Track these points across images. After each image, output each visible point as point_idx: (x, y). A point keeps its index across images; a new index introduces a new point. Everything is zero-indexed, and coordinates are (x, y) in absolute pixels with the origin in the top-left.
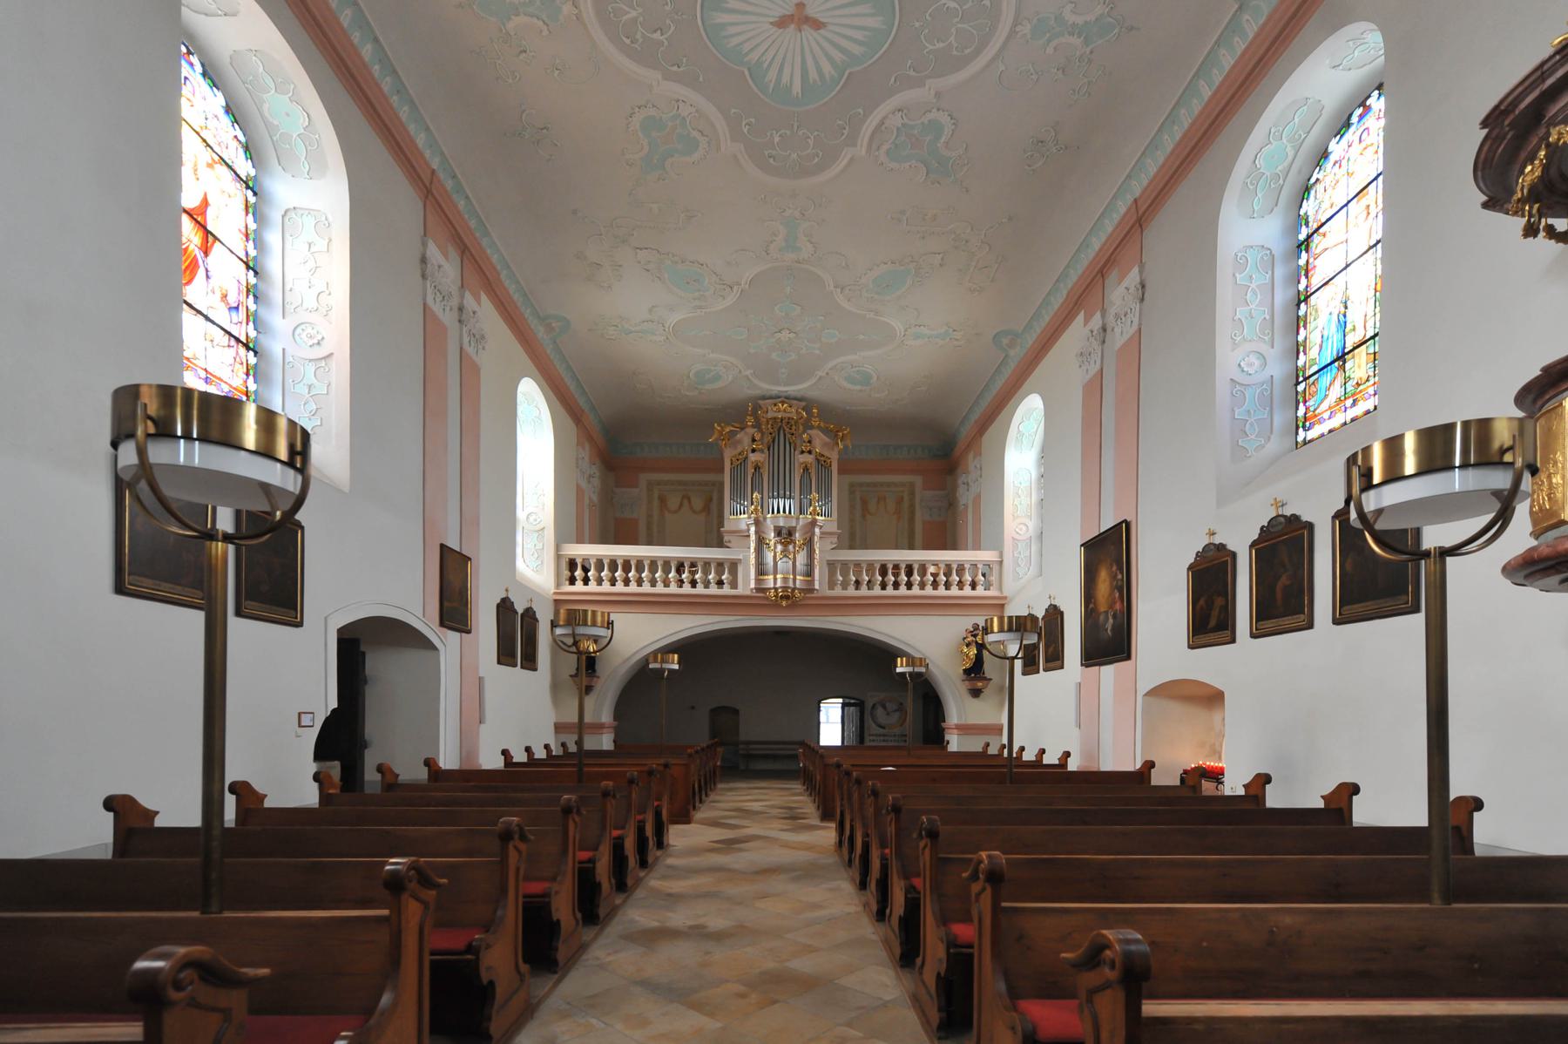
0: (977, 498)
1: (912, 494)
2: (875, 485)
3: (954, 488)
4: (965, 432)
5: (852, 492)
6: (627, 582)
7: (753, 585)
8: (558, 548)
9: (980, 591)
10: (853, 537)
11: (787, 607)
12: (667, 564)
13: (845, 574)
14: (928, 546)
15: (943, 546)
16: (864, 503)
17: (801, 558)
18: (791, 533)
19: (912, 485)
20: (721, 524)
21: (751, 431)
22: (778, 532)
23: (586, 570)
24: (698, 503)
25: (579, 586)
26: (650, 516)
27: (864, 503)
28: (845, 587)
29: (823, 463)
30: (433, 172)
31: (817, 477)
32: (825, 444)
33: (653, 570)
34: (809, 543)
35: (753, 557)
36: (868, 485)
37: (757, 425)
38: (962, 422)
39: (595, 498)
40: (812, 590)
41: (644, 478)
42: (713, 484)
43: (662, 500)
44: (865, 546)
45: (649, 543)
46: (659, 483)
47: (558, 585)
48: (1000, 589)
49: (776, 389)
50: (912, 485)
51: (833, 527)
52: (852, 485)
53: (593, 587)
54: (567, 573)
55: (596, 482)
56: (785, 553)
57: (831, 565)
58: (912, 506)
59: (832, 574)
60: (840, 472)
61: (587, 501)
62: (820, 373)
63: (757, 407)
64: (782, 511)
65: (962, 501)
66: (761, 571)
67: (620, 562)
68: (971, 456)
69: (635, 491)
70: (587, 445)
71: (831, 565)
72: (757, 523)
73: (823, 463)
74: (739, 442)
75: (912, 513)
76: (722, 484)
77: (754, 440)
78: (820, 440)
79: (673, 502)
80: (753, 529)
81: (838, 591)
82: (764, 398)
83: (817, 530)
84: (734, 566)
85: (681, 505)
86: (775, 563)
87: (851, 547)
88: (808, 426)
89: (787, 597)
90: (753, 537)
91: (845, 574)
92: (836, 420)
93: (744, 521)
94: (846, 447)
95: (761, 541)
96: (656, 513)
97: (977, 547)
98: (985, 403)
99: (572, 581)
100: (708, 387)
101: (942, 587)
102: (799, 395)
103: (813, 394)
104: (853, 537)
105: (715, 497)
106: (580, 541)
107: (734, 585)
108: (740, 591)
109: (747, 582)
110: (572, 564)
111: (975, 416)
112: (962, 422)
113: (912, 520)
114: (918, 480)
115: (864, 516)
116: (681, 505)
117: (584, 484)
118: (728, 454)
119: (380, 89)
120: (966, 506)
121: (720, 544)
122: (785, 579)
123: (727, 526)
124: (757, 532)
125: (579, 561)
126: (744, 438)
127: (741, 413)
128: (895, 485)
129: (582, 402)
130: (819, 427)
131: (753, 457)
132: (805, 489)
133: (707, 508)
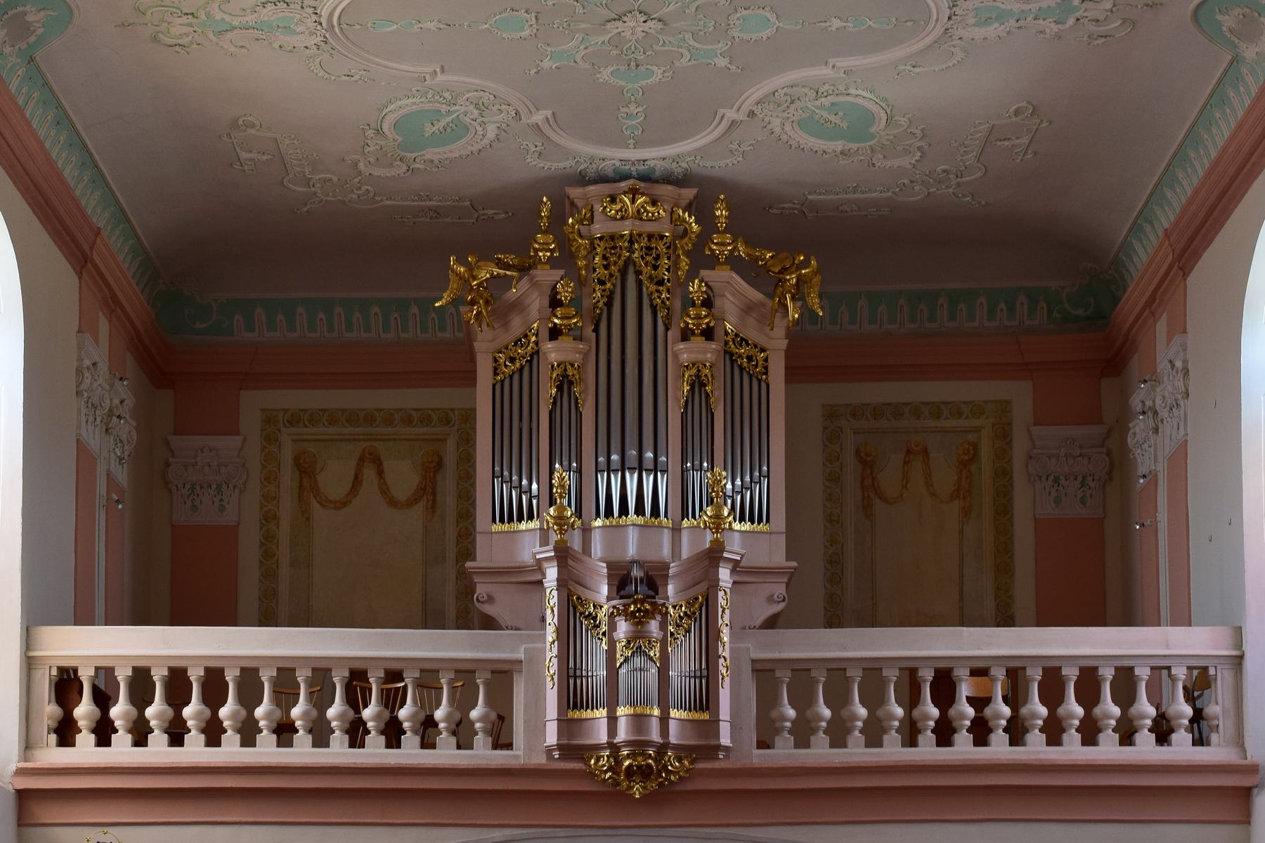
0: (1179, 458)
1: (1004, 435)
2: (897, 411)
3: (1124, 417)
4: (1145, 254)
5: (832, 436)
6: (213, 734)
7: (551, 738)
8: (28, 641)
9: (1181, 748)
10: (837, 584)
11: (647, 799)
12: (321, 674)
13: (803, 701)
14: (1053, 613)
15: (1095, 613)
16: (867, 464)
17: (682, 663)
18: (654, 580)
19: (1004, 408)
20: (467, 551)
21: (546, 275)
22: (621, 581)
23: (103, 700)
24: (403, 475)
25: (85, 750)
26: (269, 518)
27: (867, 464)
28: (802, 741)
29: (742, 365)
30: (98, 232)
31: (725, 415)
32: (748, 308)
33: (285, 695)
34: (702, 610)
35: (552, 652)
36: (878, 411)
37: (565, 258)
38: (1136, 228)
39: (122, 476)
40: (712, 750)
41: (254, 404)
42: (446, 420)
43: (305, 469)
44: (869, 618)
45: (267, 618)
46: (294, 419)
47: (28, 745)
48: (1239, 741)
49: (614, 156)
50: (1004, 408)
51: (774, 553)
52: (831, 413)
53: (122, 750)
54: (49, 710)
55: (126, 429)
56: (638, 640)
57: (764, 673)
58: (1003, 475)
59: (767, 700)
60: (793, 374)
61: (101, 487)
62: (731, 114)
63: (563, 206)
64: (636, 513)
65: (1144, 463)
66: (574, 697)
67: (195, 674)
68: (1161, 326)
69: (227, 444)
70: (104, 326)
71: (764, 673)
72: (563, 555)
73: (742, 365)
74: (518, 306)
75: (1004, 497)
76: (469, 416)
77: (555, 303)
78: (734, 292)
79: (334, 475)
80: (552, 573)
81: (784, 752)
82: (583, 180)
83: (724, 574)
84: (502, 677)
85: (357, 481)
86: (613, 671)
87: (833, 621)
88: (701, 259)
89: (644, 773)
90: (552, 598)
91: (803, 701)
92: (773, 228)
93: (529, 542)
94: (808, 313)
95: (574, 608)
96: (286, 508)
97: (1183, 618)
98: (1189, 181)
99: (65, 732)
100: (432, 153)
101: (1072, 737)
102: (677, 170)
103: (720, 165)
104: (837, 584)
105: (450, 459)
106: (83, 617)
107: (501, 741)
108: (518, 755)
109: (537, 728)
110: (66, 685)
111: (1166, 217)
112: (1136, 228)
113: (1004, 509)
114: (1019, 395)
115: (866, 508)
116: (357, 481)
117: (94, 438)
118: (486, 344)
119: (16, 104)
120: (1152, 478)
121: (470, 617)
122: (639, 721)
123: (486, 555)
124: (561, 583)
125: (86, 675)
126: (529, 295)
127: (513, 224)
128: (956, 410)
129: (91, 202)
130: (734, 262)
131: (553, 352)
132: (696, 445)
133: (427, 491)
